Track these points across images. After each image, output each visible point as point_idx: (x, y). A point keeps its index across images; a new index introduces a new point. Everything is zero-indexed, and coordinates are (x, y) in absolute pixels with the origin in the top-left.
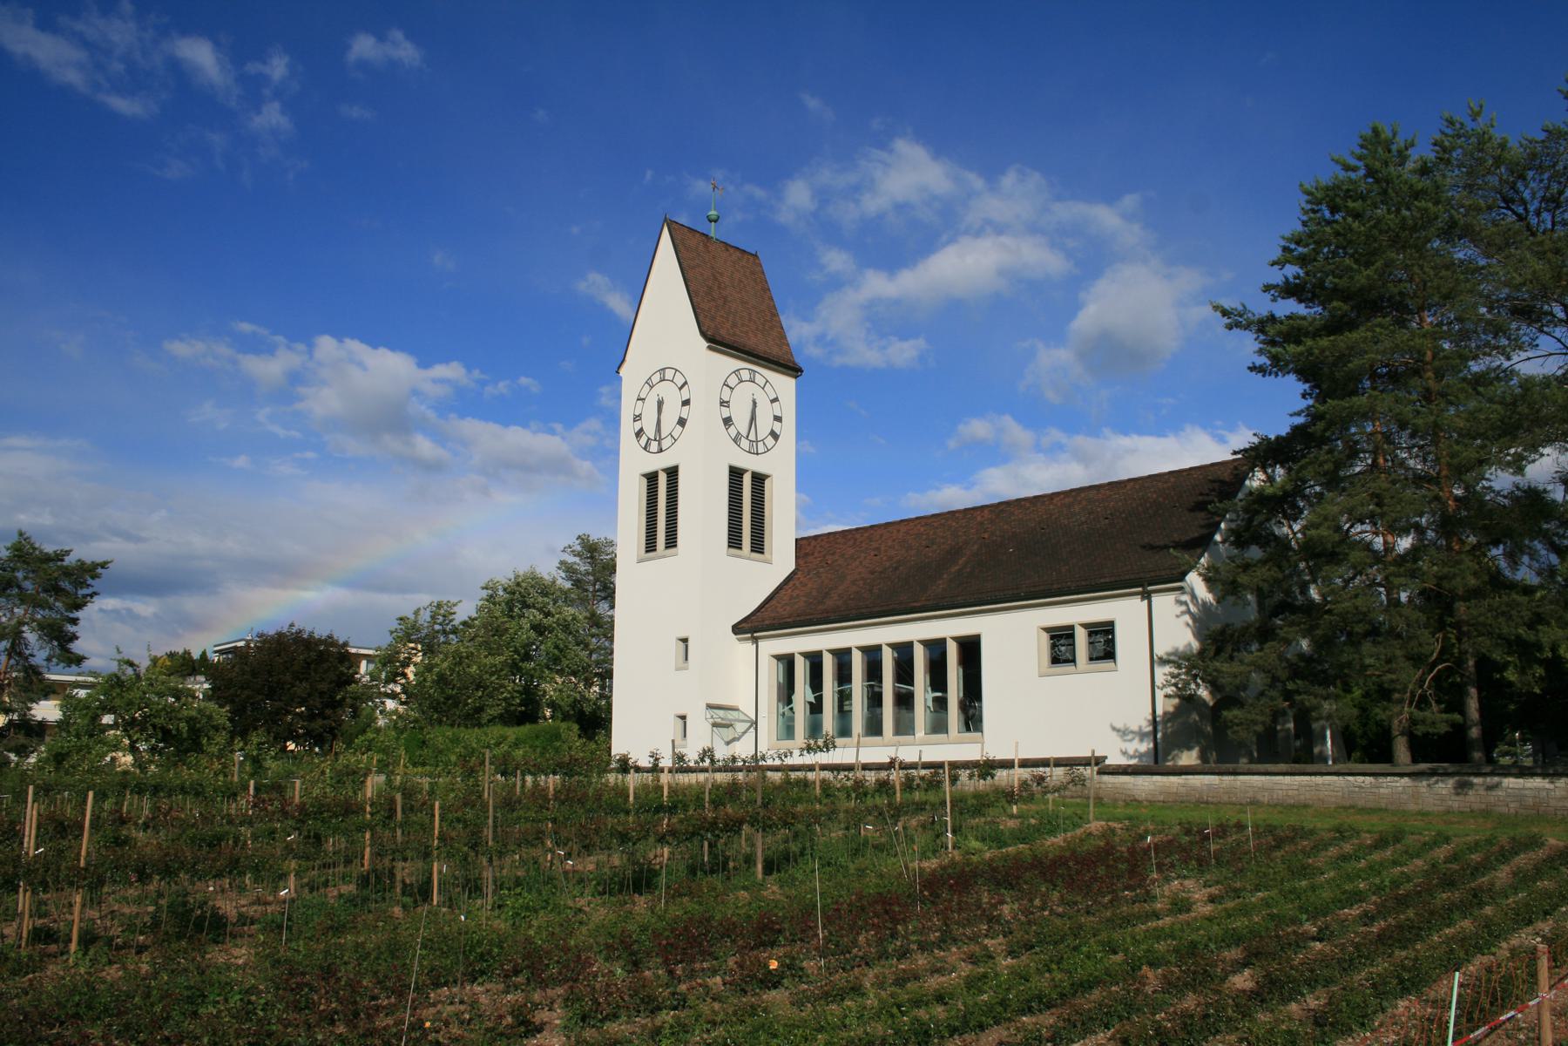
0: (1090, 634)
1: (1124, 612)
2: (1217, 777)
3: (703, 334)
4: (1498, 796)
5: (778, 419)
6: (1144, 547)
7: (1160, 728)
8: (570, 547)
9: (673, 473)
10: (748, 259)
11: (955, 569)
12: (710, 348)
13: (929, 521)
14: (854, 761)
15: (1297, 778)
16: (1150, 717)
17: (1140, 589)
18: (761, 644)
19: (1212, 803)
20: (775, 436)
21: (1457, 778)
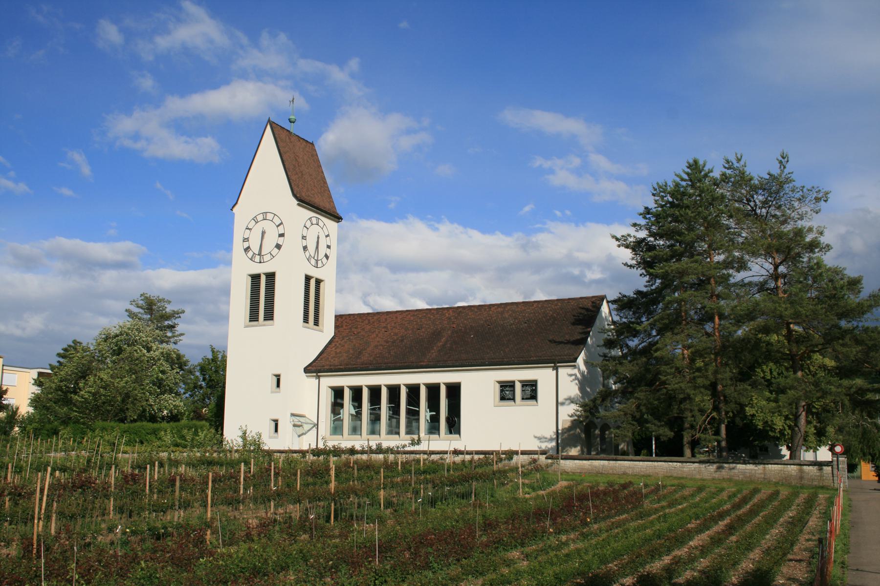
0: (523, 386)
1: (543, 376)
2: (607, 462)
3: (295, 195)
4: (735, 472)
5: (329, 247)
6: (550, 341)
7: (560, 436)
8: (134, 301)
9: (271, 277)
10: (309, 147)
11: (440, 344)
12: (298, 205)
13: (416, 313)
14: (427, 449)
15: (646, 463)
16: (555, 431)
17: (553, 365)
18: (322, 379)
19: (604, 474)
20: (327, 257)
21: (718, 464)
